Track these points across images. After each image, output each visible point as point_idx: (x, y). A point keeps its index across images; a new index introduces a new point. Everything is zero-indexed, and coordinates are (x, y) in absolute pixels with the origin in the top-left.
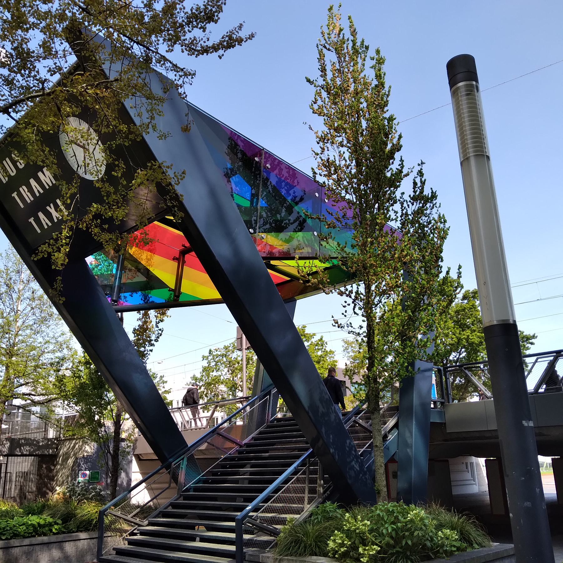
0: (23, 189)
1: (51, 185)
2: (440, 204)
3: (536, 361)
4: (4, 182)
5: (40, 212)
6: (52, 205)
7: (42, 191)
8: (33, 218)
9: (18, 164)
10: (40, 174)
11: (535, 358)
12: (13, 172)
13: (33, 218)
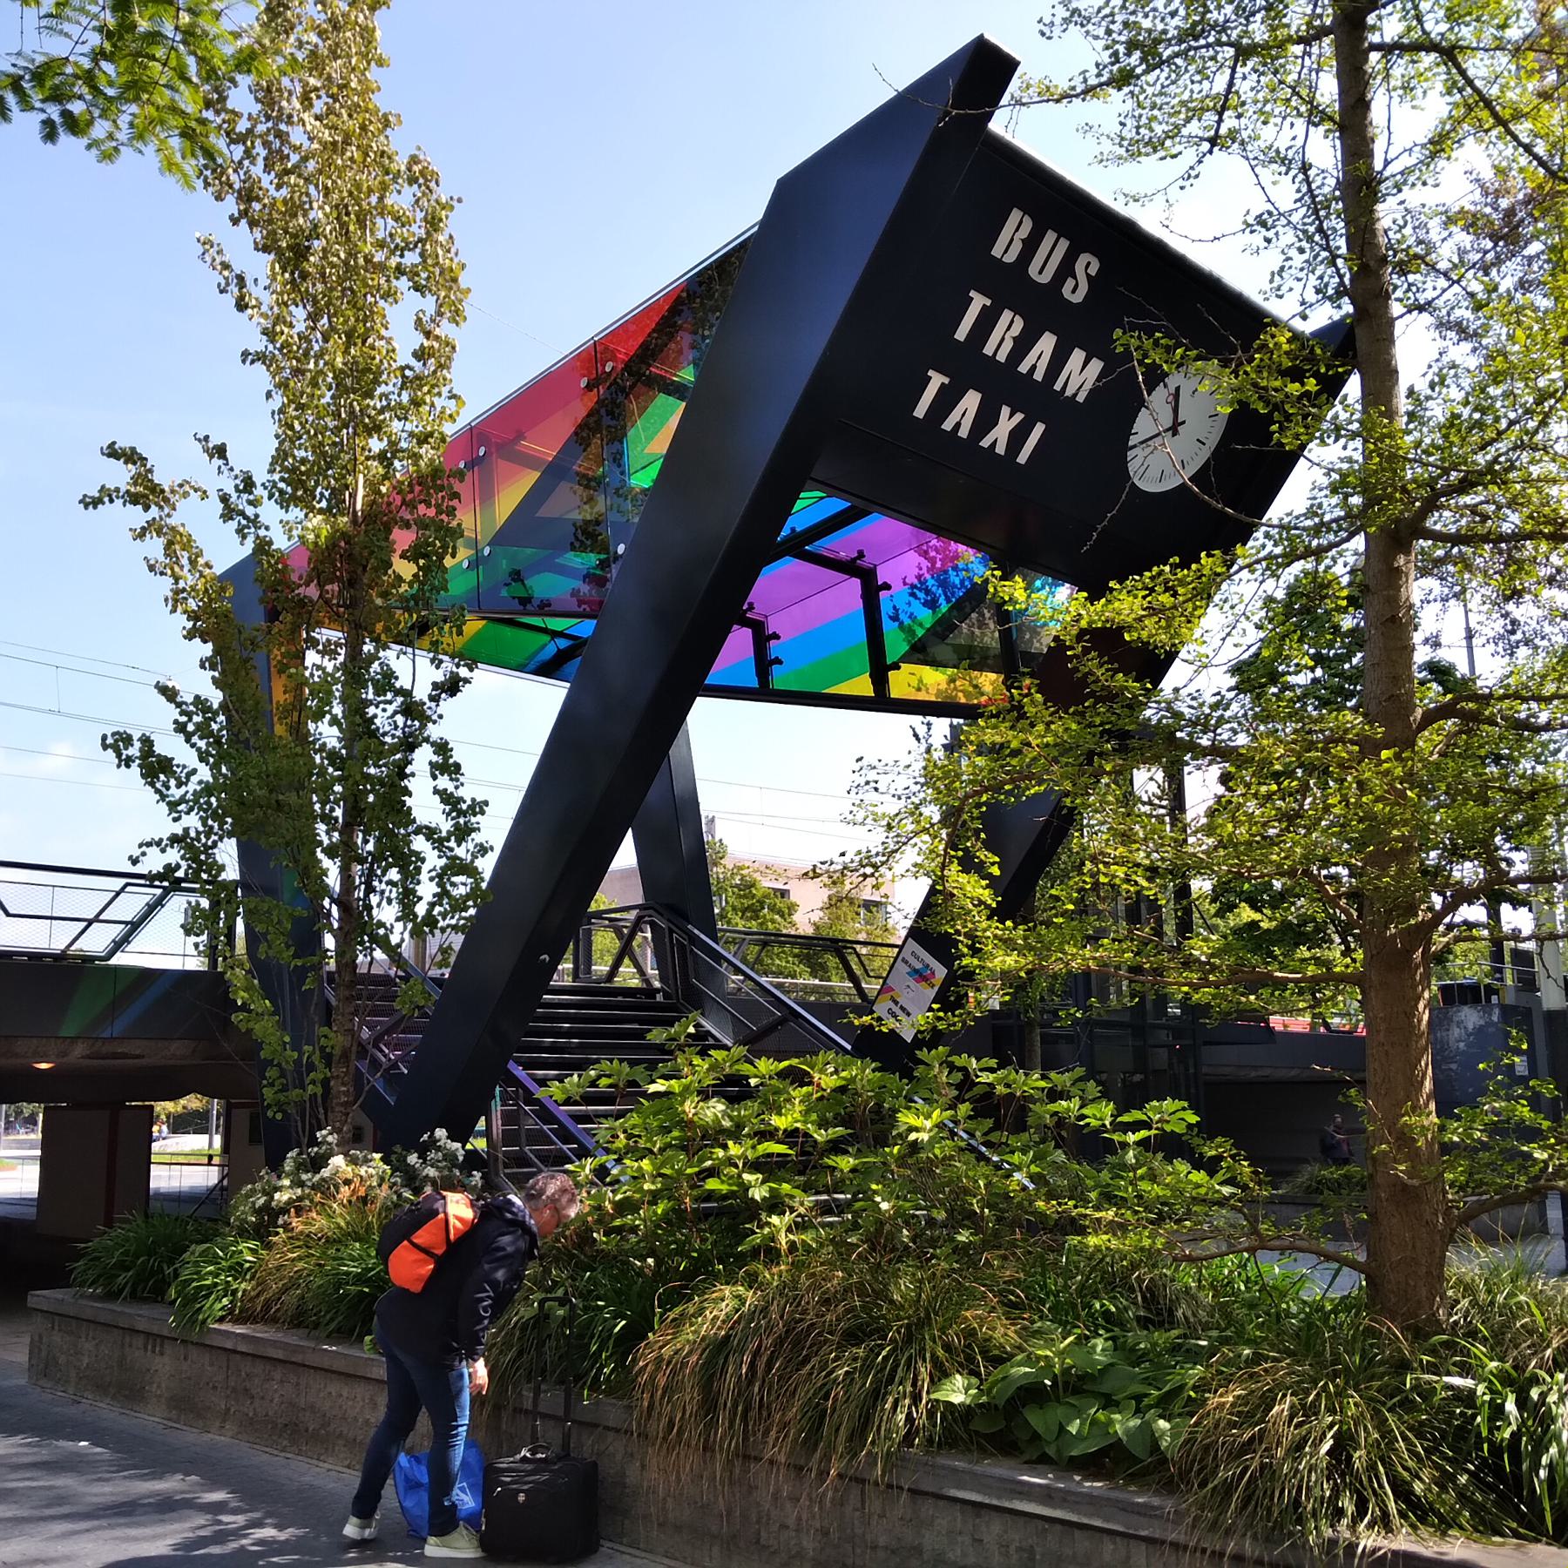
0: (1012, 322)
1: (1069, 393)
2: (113, 452)
3: (123, 889)
4: (997, 251)
5: (978, 396)
6: (1019, 417)
7: (1039, 376)
8: (946, 380)
9: (1070, 283)
10: (1078, 356)
11: (123, 881)
12: (1040, 272)
13: (946, 380)
